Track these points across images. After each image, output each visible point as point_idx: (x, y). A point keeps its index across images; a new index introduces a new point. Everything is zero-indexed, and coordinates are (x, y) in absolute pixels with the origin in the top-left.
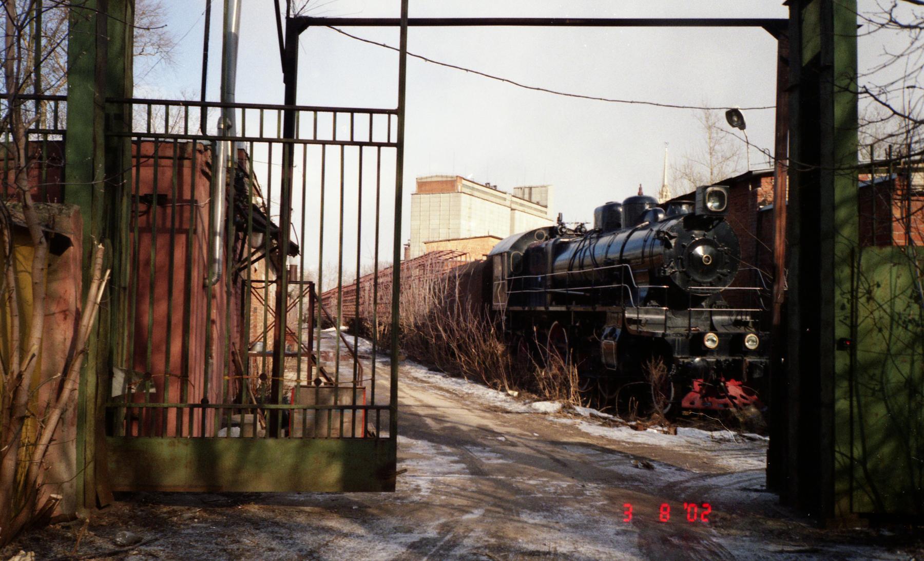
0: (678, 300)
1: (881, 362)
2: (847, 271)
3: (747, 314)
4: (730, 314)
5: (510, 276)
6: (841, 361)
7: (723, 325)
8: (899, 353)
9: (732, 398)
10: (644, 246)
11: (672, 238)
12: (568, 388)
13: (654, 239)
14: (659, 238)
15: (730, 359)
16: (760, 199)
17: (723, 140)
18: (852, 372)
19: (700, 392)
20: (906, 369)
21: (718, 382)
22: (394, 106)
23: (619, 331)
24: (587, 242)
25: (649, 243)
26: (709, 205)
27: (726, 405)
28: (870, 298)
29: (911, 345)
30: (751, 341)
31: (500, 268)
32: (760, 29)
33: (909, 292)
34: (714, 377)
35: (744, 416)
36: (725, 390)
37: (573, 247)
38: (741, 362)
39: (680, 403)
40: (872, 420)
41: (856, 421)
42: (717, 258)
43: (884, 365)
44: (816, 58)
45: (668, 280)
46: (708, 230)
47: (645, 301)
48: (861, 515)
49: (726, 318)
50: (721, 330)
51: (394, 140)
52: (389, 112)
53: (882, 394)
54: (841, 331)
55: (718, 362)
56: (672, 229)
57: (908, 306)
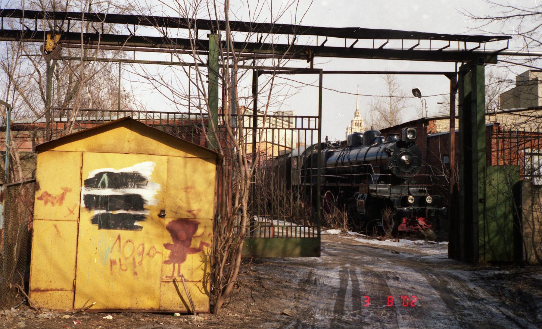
0: (396, 181)
1: (494, 207)
2: (482, 175)
3: (425, 187)
4: (417, 187)
5: (303, 167)
6: (480, 207)
7: (414, 192)
8: (501, 204)
9: (421, 226)
10: (377, 156)
11: (391, 152)
12: (343, 222)
13: (382, 152)
14: (385, 152)
15: (420, 208)
16: (428, 131)
17: (397, 90)
18: (485, 210)
19: (406, 223)
20: (503, 209)
21: (414, 219)
22: (317, 115)
23: (366, 195)
24: (345, 152)
25: (379, 154)
26: (408, 136)
27: (418, 229)
28: (490, 185)
29: (505, 201)
30: (429, 200)
31: (296, 163)
32: (443, 76)
33: (504, 182)
34: (412, 216)
35: (427, 234)
36: (417, 222)
37: (337, 154)
38: (426, 209)
39: (397, 229)
40: (491, 228)
41: (486, 228)
42: (411, 161)
43: (495, 208)
44: (470, 94)
45: (390, 171)
46: (408, 148)
47: (378, 182)
48: (489, 262)
49: (415, 189)
50: (414, 195)
51: (317, 127)
52: (316, 117)
53: (495, 219)
54: (480, 196)
55: (414, 209)
56: (391, 147)
57: (504, 187)
